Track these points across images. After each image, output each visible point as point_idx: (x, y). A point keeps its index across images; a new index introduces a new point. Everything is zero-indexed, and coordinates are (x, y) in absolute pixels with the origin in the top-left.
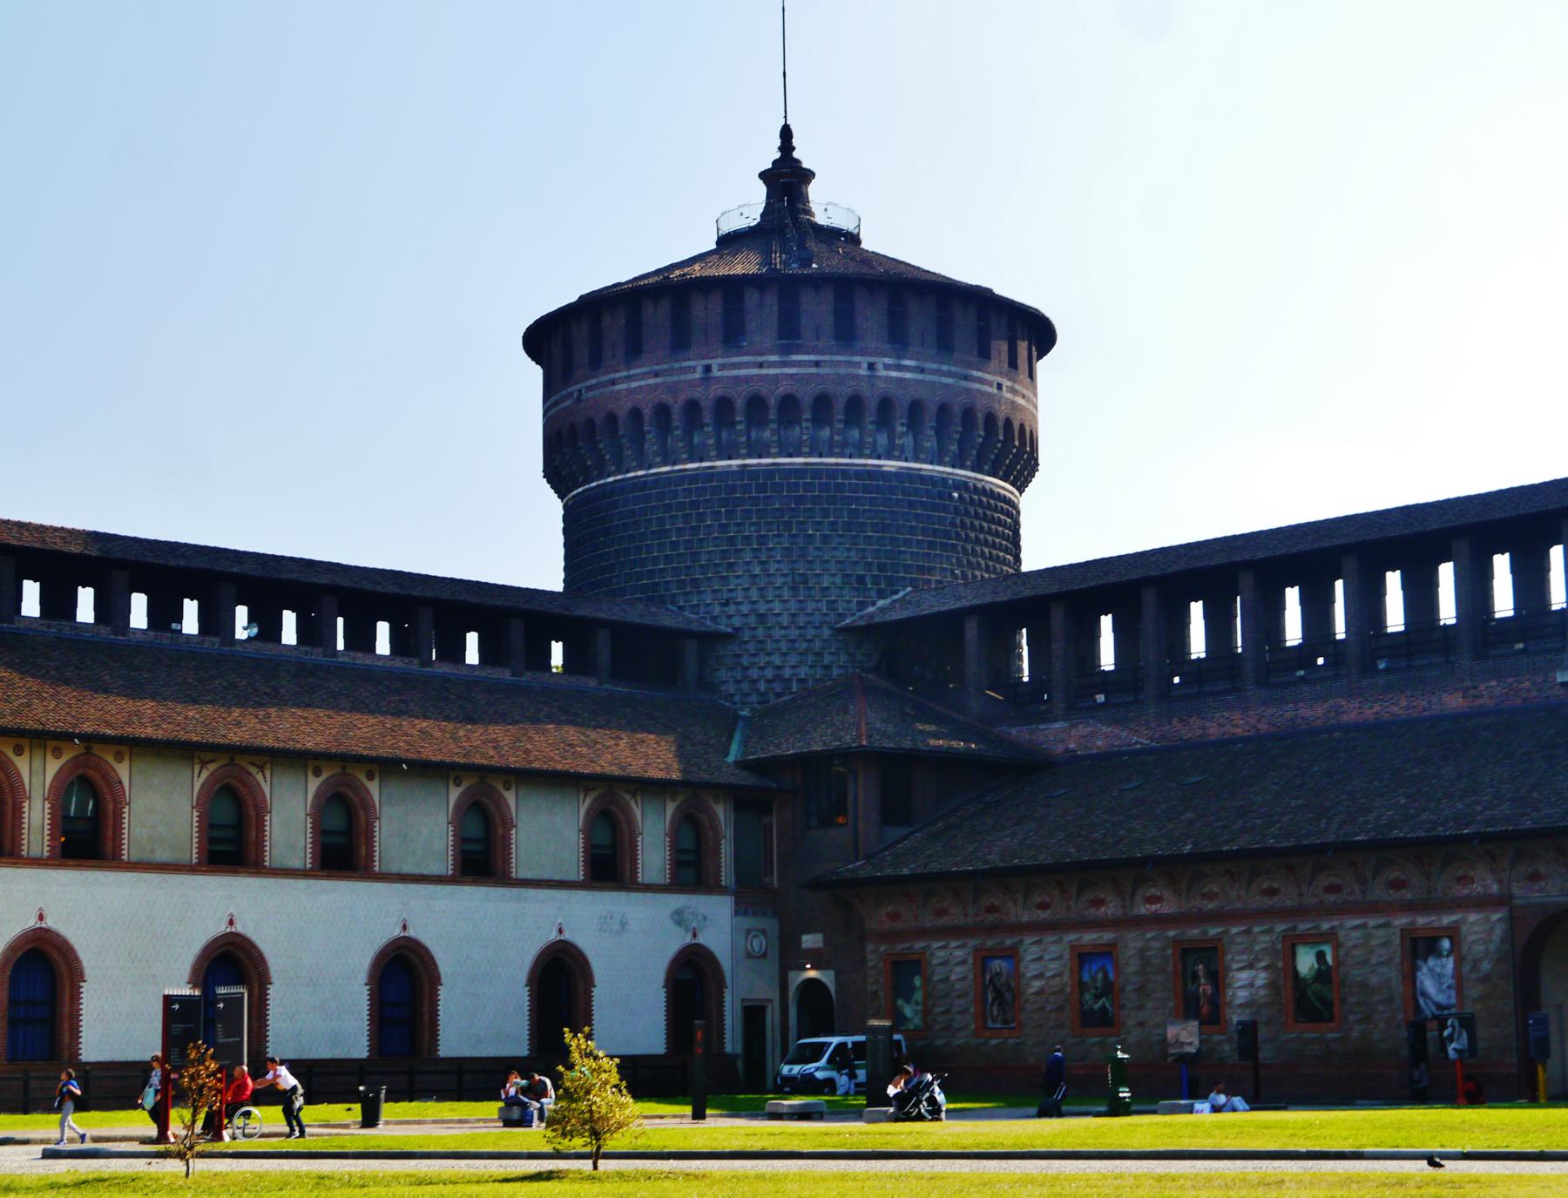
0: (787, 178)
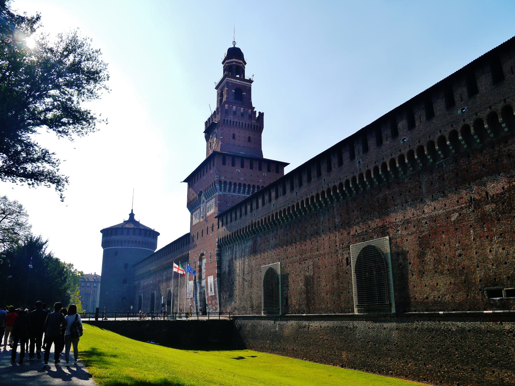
0: (132, 215)
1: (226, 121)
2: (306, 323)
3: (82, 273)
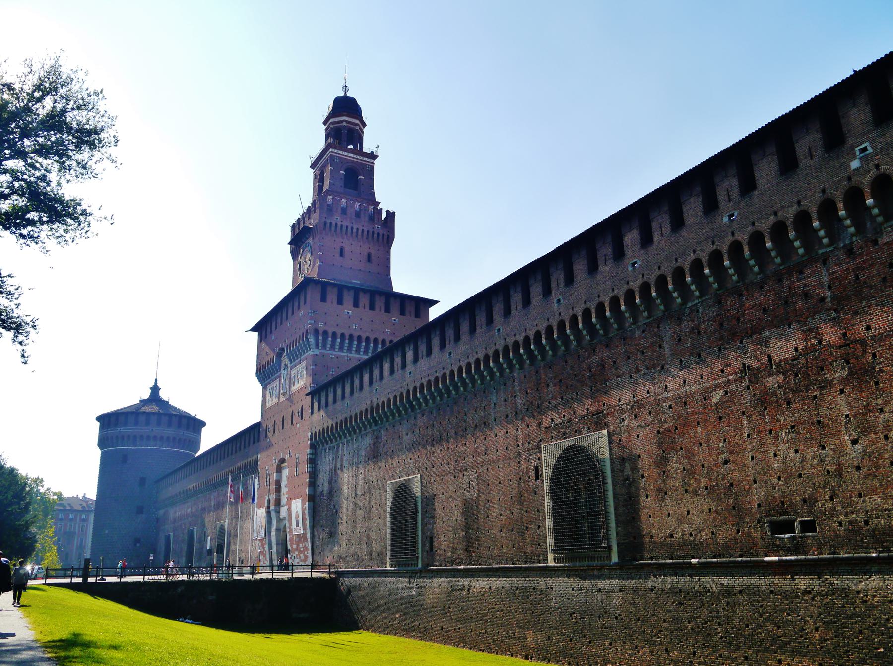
0: (155, 390)
1: (328, 225)
2: (464, 582)
3: (59, 495)
